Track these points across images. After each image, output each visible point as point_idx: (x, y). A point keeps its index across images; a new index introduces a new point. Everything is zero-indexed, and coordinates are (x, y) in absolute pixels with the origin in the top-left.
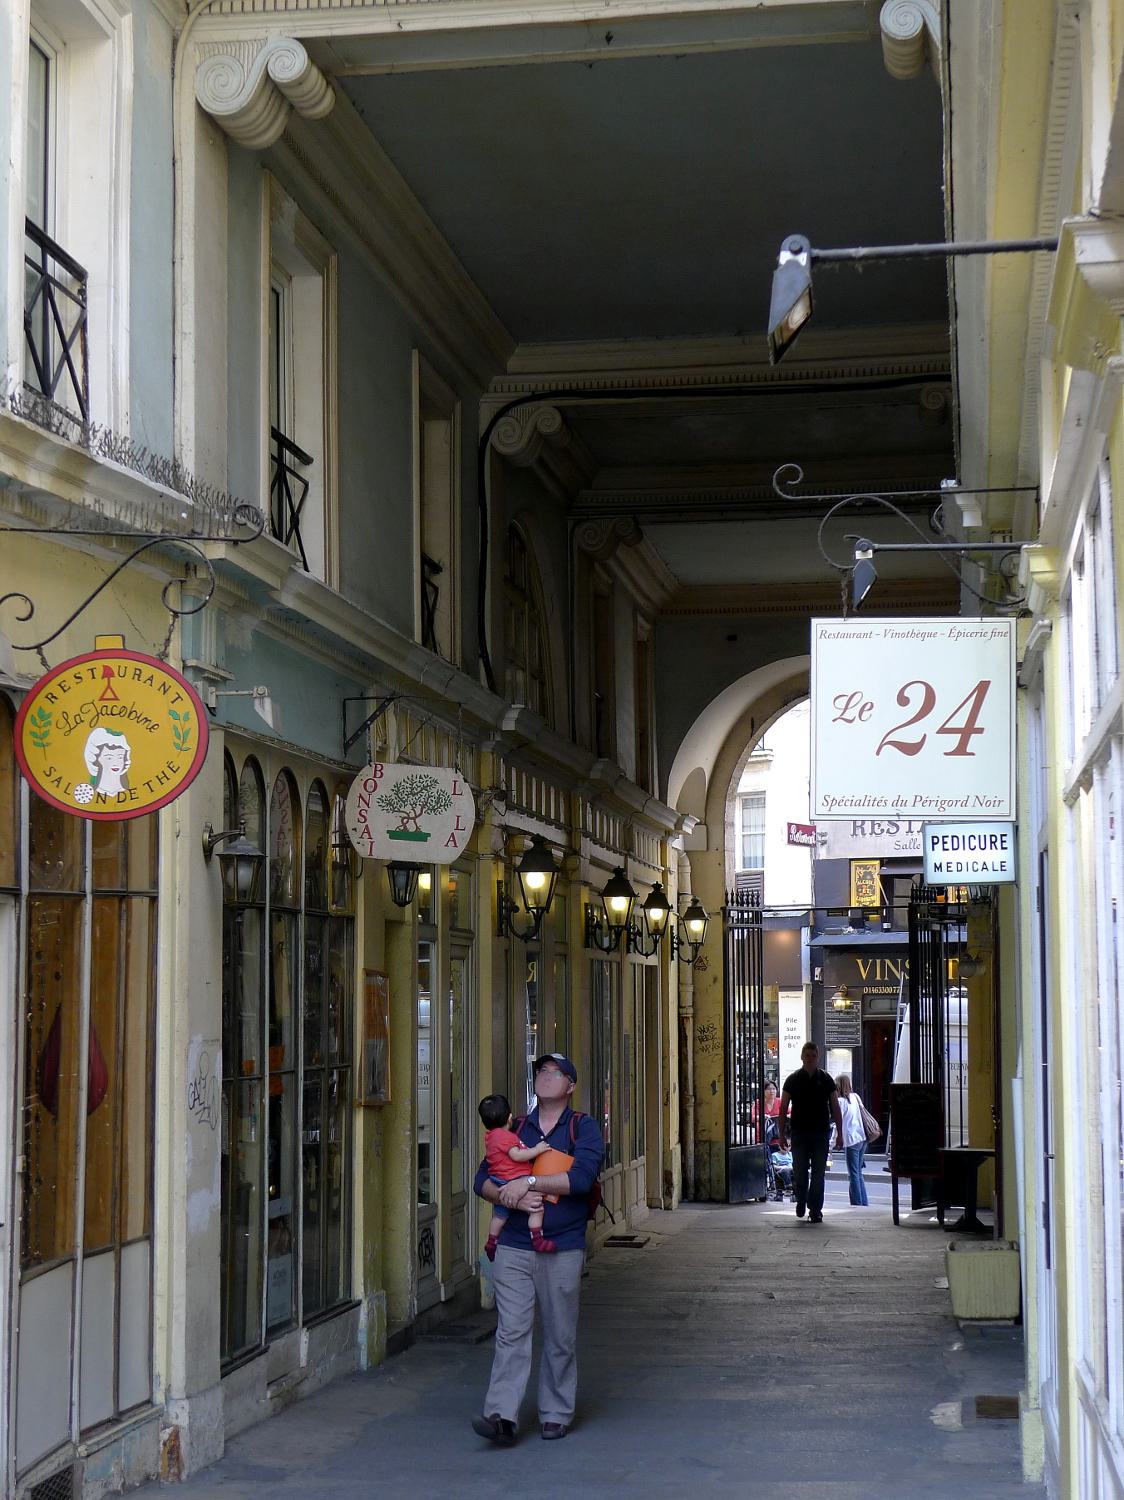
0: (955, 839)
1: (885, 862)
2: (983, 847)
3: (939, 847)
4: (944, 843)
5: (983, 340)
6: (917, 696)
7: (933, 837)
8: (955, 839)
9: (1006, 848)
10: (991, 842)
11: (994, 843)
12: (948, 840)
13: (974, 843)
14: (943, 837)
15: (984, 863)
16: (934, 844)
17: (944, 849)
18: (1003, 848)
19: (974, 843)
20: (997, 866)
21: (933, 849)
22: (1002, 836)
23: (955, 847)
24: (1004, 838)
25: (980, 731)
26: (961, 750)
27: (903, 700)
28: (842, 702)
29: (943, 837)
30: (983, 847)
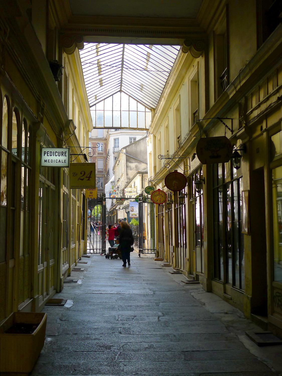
0: (51, 153)
1: (199, 283)
2: (59, 155)
3: (46, 155)
4: (48, 154)
5: (124, 119)
6: (83, 173)
7: (44, 152)
8: (51, 153)
9: (66, 156)
10: (62, 154)
11: (63, 154)
12: (49, 153)
13: (57, 154)
14: (48, 152)
15: (60, 160)
16: (44, 154)
17: (48, 156)
18: (65, 156)
19: (57, 154)
20: (63, 161)
21: (44, 156)
22: (65, 152)
23: (51, 155)
24: (66, 153)
25: (91, 177)
26: (89, 180)
27: (81, 173)
28: (73, 174)
29: (48, 152)
30: (59, 155)
